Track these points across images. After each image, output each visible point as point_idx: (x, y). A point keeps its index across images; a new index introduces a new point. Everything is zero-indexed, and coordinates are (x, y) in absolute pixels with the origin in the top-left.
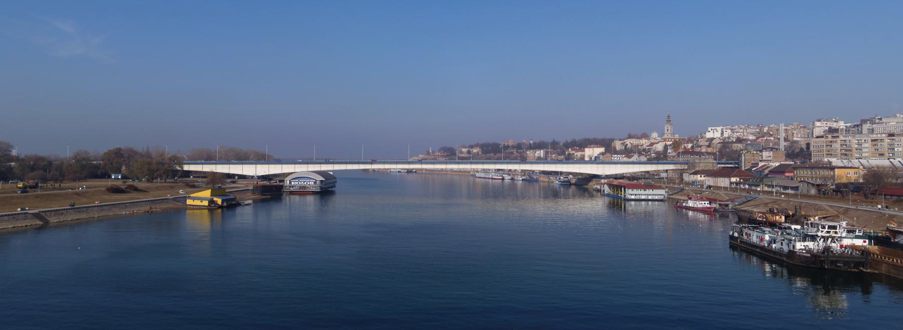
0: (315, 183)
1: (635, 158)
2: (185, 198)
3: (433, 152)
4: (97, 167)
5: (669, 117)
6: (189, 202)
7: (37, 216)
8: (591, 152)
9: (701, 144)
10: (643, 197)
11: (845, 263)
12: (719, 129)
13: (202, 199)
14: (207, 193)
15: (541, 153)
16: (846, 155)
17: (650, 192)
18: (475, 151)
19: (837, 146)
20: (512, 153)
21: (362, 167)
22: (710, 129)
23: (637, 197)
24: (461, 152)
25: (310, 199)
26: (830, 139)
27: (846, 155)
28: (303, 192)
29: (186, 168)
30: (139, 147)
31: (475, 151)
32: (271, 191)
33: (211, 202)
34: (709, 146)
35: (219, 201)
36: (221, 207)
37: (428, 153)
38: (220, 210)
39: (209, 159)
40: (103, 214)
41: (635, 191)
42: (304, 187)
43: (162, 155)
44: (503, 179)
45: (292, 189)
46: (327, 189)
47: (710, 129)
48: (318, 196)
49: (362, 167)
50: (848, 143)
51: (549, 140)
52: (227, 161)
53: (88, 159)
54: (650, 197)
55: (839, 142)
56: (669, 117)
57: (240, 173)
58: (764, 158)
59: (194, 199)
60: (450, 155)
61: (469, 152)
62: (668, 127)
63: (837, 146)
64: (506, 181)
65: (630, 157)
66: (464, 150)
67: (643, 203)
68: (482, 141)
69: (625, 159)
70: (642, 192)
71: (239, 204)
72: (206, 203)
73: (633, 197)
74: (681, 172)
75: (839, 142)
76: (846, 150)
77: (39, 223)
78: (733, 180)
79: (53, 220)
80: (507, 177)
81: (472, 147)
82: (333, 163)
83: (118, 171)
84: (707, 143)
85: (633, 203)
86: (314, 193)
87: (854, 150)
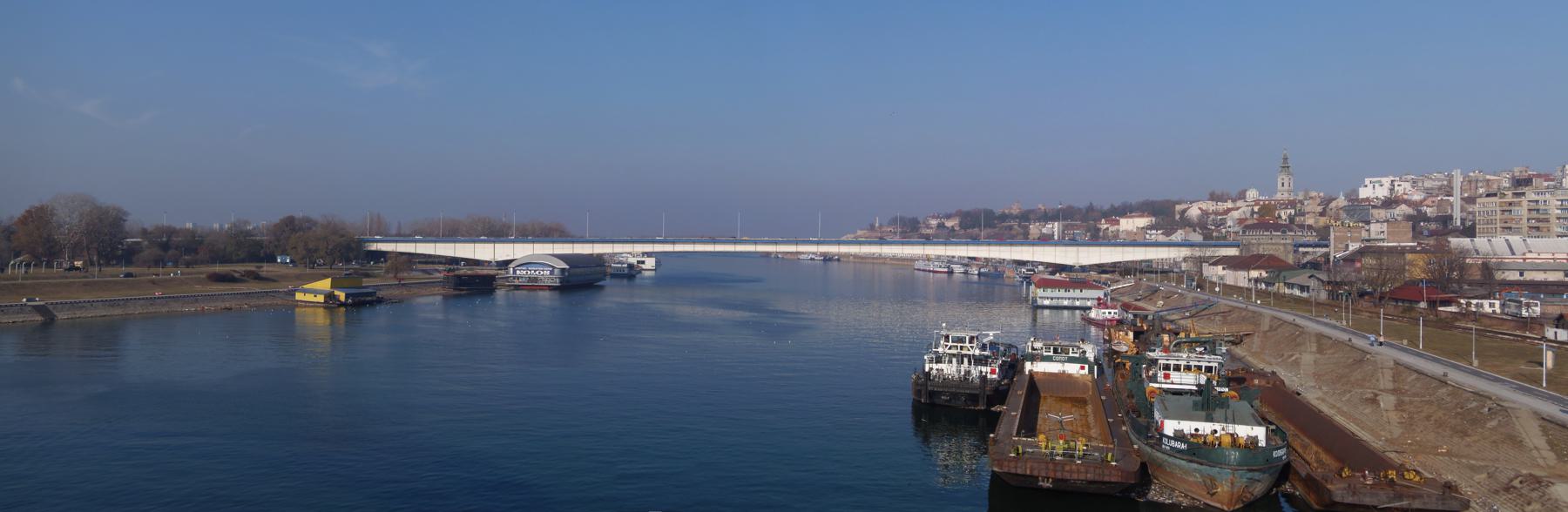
0: (552, 273)
1: (1178, 236)
2: (292, 293)
3: (881, 226)
4: (259, 244)
5: (1286, 159)
6: (299, 296)
7: (38, 309)
8: (1128, 224)
9: (1307, 209)
10: (1066, 303)
11: (954, 396)
12: (1386, 181)
13: (316, 292)
14: (325, 284)
15: (1055, 228)
16: (1538, 228)
17: (1076, 293)
18: (949, 224)
19: (1522, 211)
20: (1011, 228)
21: (679, 248)
22: (1367, 181)
23: (1054, 303)
24: (928, 227)
25: (547, 294)
26: (1509, 199)
27: (1538, 228)
28: (533, 286)
29: (374, 247)
30: (315, 215)
31: (949, 224)
32: (475, 284)
33: (330, 297)
34: (1322, 214)
35: (342, 296)
36: (342, 304)
37: (872, 227)
38: (343, 309)
39: (452, 234)
40: (151, 309)
41: (1049, 292)
42: (536, 279)
43: (52, 215)
44: (951, 272)
45: (516, 282)
46: (582, 279)
47: (1367, 181)
48: (556, 294)
49: (679, 248)
50: (1541, 206)
51: (1082, 204)
52: (472, 236)
53: (249, 233)
54: (1078, 303)
55: (1525, 204)
56: (1286, 159)
57: (470, 256)
58: (1373, 236)
59: (305, 291)
60: (910, 230)
61: (941, 226)
62: (1282, 178)
63: (1522, 211)
64: (956, 275)
65: (1167, 234)
66: (934, 222)
67: (1066, 312)
68: (967, 207)
69: (1162, 238)
70: (1062, 293)
71: (380, 301)
72: (321, 298)
73: (1047, 302)
74: (1200, 261)
75: (1525, 204)
76: (1538, 220)
77: (39, 318)
78: (1255, 274)
79: (61, 316)
80: (958, 269)
81: (948, 217)
82: (613, 242)
83: (284, 253)
84: (1320, 209)
85: (1046, 312)
86: (551, 288)
87: (1553, 220)
